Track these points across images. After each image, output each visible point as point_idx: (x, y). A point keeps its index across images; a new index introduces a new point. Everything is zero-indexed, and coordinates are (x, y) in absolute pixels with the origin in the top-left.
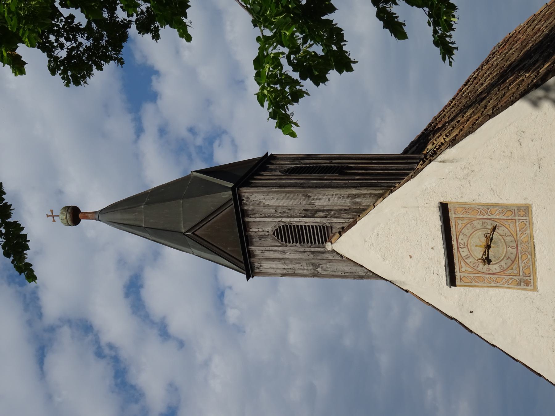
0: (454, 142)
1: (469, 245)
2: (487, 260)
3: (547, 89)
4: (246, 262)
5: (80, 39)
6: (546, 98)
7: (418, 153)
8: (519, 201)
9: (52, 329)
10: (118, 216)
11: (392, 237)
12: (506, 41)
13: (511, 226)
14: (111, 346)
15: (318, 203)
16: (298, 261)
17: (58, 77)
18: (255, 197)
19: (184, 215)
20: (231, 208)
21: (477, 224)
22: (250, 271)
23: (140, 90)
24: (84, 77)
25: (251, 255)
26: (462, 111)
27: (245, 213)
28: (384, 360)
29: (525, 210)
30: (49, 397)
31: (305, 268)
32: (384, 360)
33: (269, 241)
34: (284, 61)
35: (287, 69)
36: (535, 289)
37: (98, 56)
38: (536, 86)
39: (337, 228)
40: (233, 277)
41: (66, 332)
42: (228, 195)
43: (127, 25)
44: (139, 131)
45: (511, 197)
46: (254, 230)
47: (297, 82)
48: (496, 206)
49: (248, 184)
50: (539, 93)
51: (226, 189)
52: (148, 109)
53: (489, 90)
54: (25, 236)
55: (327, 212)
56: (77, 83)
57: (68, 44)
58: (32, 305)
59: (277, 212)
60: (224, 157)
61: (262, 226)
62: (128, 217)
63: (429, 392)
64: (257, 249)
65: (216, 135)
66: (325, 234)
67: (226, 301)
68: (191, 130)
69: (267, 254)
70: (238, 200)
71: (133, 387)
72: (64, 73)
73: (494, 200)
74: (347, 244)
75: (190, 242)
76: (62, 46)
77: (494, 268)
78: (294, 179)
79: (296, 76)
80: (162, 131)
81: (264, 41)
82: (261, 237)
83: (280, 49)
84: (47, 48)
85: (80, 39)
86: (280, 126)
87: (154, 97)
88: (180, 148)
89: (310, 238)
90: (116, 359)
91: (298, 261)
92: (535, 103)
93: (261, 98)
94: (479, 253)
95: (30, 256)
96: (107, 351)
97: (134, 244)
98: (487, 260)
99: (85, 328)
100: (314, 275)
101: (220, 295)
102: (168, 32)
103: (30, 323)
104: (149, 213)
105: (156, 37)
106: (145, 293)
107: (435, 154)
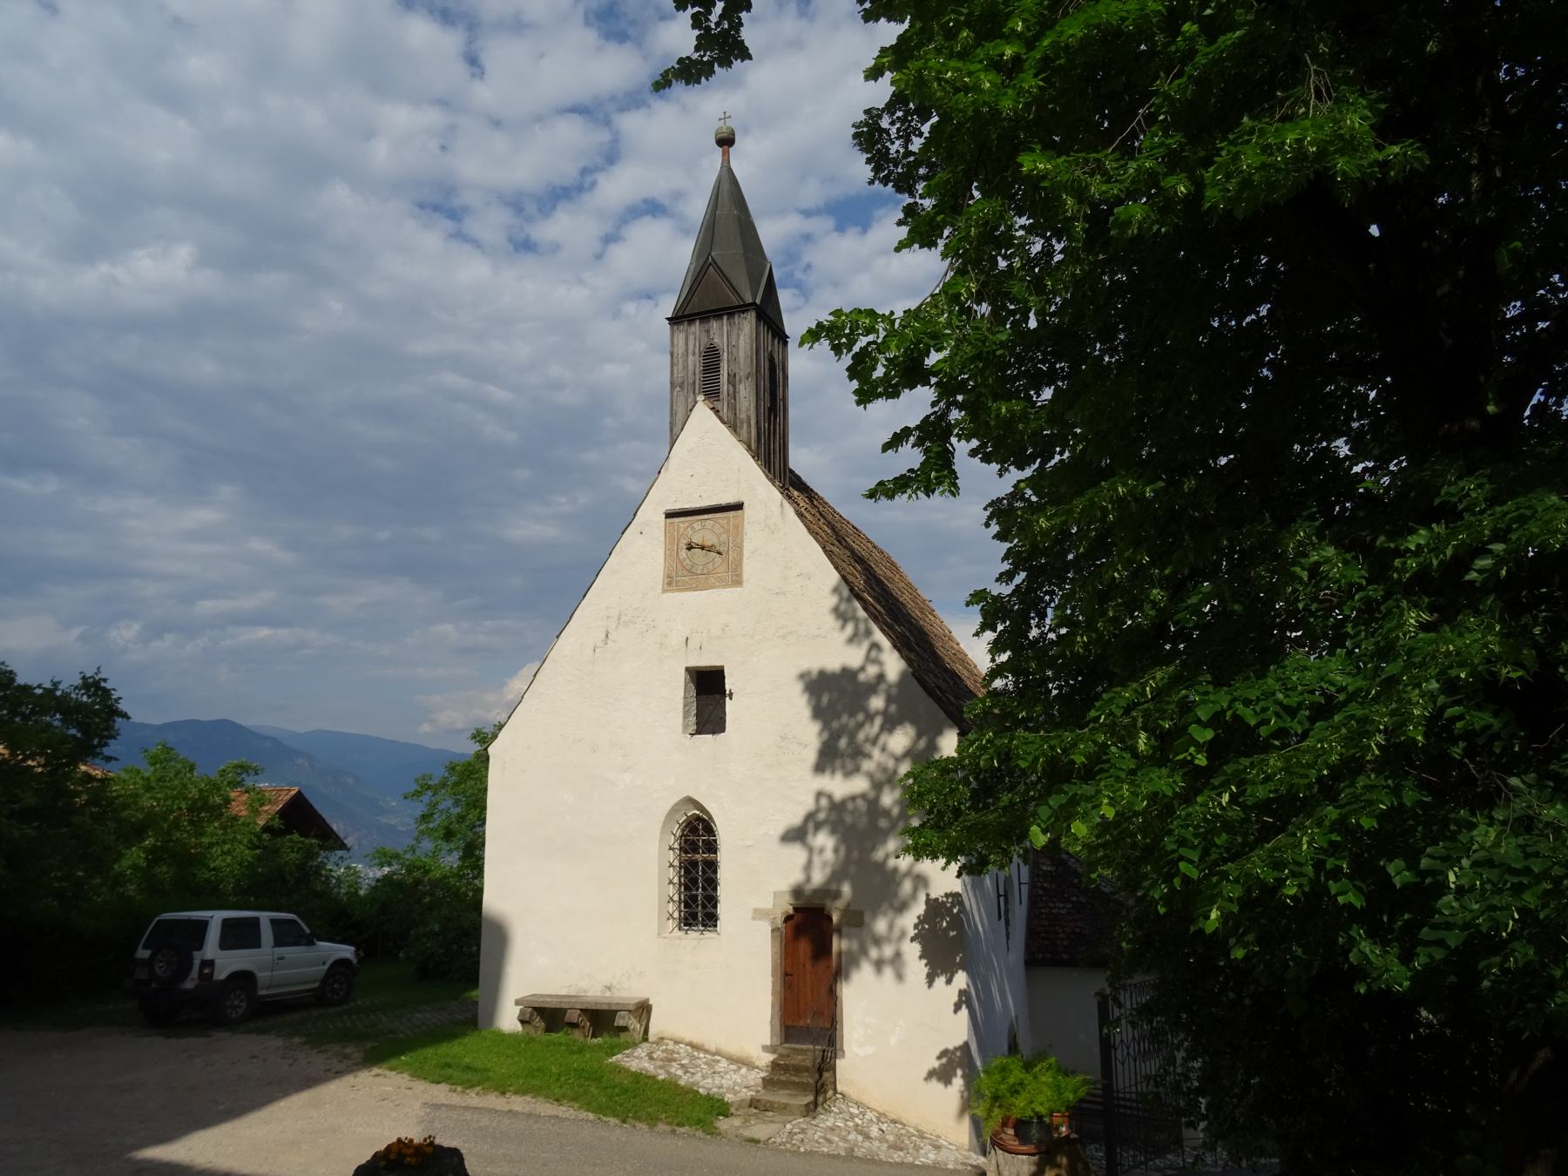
0: (800, 515)
1: (703, 530)
2: (690, 547)
3: (848, 600)
4: (683, 317)
5: (898, 143)
6: (841, 599)
7: (790, 483)
8: (745, 576)
9: (607, 122)
10: (726, 186)
11: (709, 457)
12: (893, 564)
13: (723, 568)
14: (594, 184)
15: (742, 387)
16: (685, 368)
17: (863, 117)
18: (747, 325)
19: (728, 254)
20: (735, 302)
21: (724, 537)
22: (675, 320)
23: (849, 214)
24: (860, 144)
25: (691, 322)
26: (829, 524)
27: (731, 315)
28: (592, 457)
29: (737, 581)
30: (539, 118)
31: (679, 375)
32: (592, 457)
33: (705, 340)
34: (871, 338)
35: (862, 342)
36: (664, 591)
37: (880, 160)
38: (852, 590)
39: (718, 405)
40: (668, 306)
41: (604, 136)
42: (749, 300)
43: (912, 195)
44: (807, 214)
45: (748, 568)
46: (714, 324)
47: (850, 350)
48: (741, 554)
49: (759, 318)
50: (846, 592)
51: (755, 297)
52: (829, 223)
53: (848, 548)
54: (699, 82)
55: (734, 395)
56: (855, 136)
57: (894, 130)
58: (631, 101)
59: (733, 347)
60: (785, 298)
61: (719, 332)
62: (725, 196)
63: (563, 500)
64: (696, 327)
65: (804, 291)
66: (712, 394)
67: (644, 302)
68: (809, 266)
69: (691, 338)
70: (743, 308)
71: (554, 207)
72: (866, 124)
73: (746, 553)
74: (702, 413)
75: (702, 261)
76: (892, 123)
77: (684, 553)
78: (765, 364)
79: (856, 349)
80: (807, 238)
81: (889, 319)
82: (708, 331)
83: (882, 334)
84: (890, 108)
85: (898, 143)
86: (810, 331)
87: (841, 228)
88: (791, 256)
89: (709, 378)
90: (580, 189)
91: (685, 368)
92: (836, 590)
93: (837, 313)
94: (697, 539)
95: (678, 88)
96: (588, 179)
97: (697, 209)
98: (690, 547)
99: (611, 156)
100: (672, 384)
101: (648, 295)
102: (904, 231)
103: (613, 98)
104: (730, 217)
105: (900, 223)
106: (647, 220)
107: (789, 497)
